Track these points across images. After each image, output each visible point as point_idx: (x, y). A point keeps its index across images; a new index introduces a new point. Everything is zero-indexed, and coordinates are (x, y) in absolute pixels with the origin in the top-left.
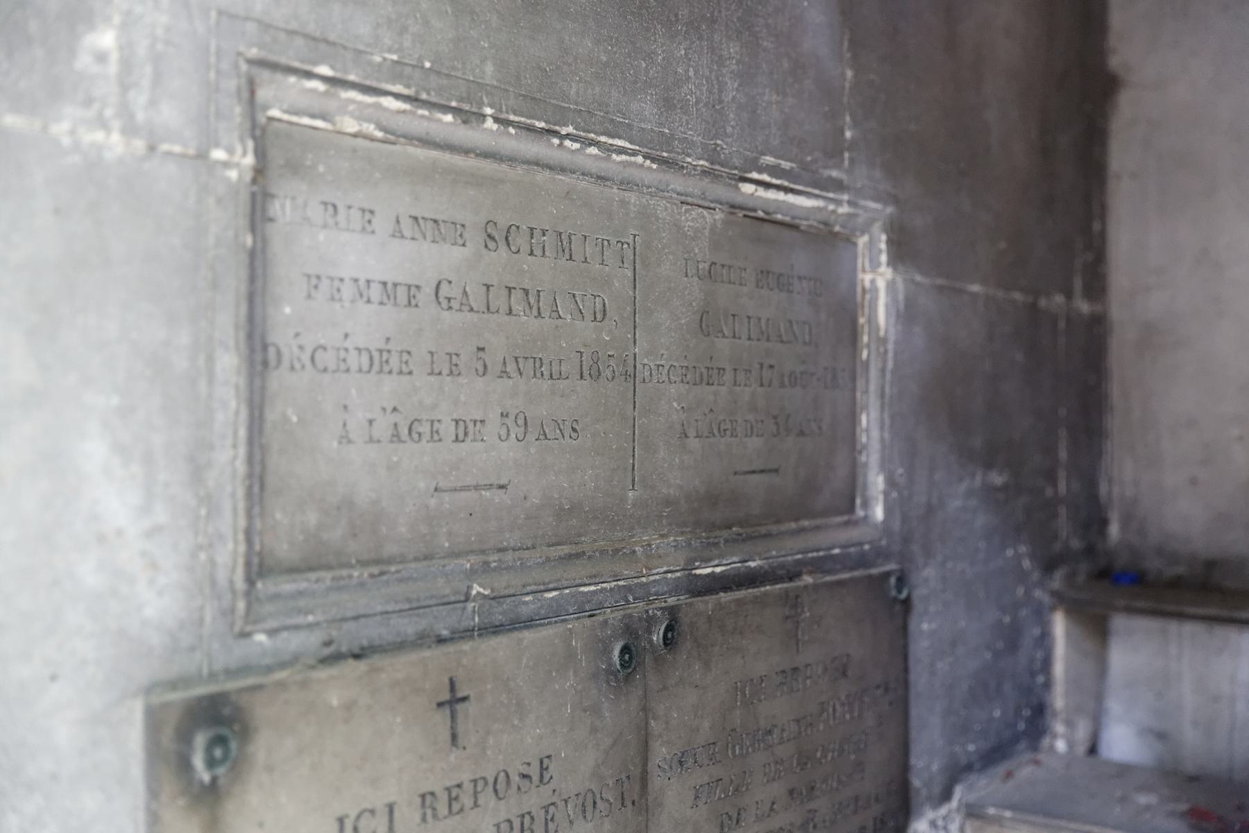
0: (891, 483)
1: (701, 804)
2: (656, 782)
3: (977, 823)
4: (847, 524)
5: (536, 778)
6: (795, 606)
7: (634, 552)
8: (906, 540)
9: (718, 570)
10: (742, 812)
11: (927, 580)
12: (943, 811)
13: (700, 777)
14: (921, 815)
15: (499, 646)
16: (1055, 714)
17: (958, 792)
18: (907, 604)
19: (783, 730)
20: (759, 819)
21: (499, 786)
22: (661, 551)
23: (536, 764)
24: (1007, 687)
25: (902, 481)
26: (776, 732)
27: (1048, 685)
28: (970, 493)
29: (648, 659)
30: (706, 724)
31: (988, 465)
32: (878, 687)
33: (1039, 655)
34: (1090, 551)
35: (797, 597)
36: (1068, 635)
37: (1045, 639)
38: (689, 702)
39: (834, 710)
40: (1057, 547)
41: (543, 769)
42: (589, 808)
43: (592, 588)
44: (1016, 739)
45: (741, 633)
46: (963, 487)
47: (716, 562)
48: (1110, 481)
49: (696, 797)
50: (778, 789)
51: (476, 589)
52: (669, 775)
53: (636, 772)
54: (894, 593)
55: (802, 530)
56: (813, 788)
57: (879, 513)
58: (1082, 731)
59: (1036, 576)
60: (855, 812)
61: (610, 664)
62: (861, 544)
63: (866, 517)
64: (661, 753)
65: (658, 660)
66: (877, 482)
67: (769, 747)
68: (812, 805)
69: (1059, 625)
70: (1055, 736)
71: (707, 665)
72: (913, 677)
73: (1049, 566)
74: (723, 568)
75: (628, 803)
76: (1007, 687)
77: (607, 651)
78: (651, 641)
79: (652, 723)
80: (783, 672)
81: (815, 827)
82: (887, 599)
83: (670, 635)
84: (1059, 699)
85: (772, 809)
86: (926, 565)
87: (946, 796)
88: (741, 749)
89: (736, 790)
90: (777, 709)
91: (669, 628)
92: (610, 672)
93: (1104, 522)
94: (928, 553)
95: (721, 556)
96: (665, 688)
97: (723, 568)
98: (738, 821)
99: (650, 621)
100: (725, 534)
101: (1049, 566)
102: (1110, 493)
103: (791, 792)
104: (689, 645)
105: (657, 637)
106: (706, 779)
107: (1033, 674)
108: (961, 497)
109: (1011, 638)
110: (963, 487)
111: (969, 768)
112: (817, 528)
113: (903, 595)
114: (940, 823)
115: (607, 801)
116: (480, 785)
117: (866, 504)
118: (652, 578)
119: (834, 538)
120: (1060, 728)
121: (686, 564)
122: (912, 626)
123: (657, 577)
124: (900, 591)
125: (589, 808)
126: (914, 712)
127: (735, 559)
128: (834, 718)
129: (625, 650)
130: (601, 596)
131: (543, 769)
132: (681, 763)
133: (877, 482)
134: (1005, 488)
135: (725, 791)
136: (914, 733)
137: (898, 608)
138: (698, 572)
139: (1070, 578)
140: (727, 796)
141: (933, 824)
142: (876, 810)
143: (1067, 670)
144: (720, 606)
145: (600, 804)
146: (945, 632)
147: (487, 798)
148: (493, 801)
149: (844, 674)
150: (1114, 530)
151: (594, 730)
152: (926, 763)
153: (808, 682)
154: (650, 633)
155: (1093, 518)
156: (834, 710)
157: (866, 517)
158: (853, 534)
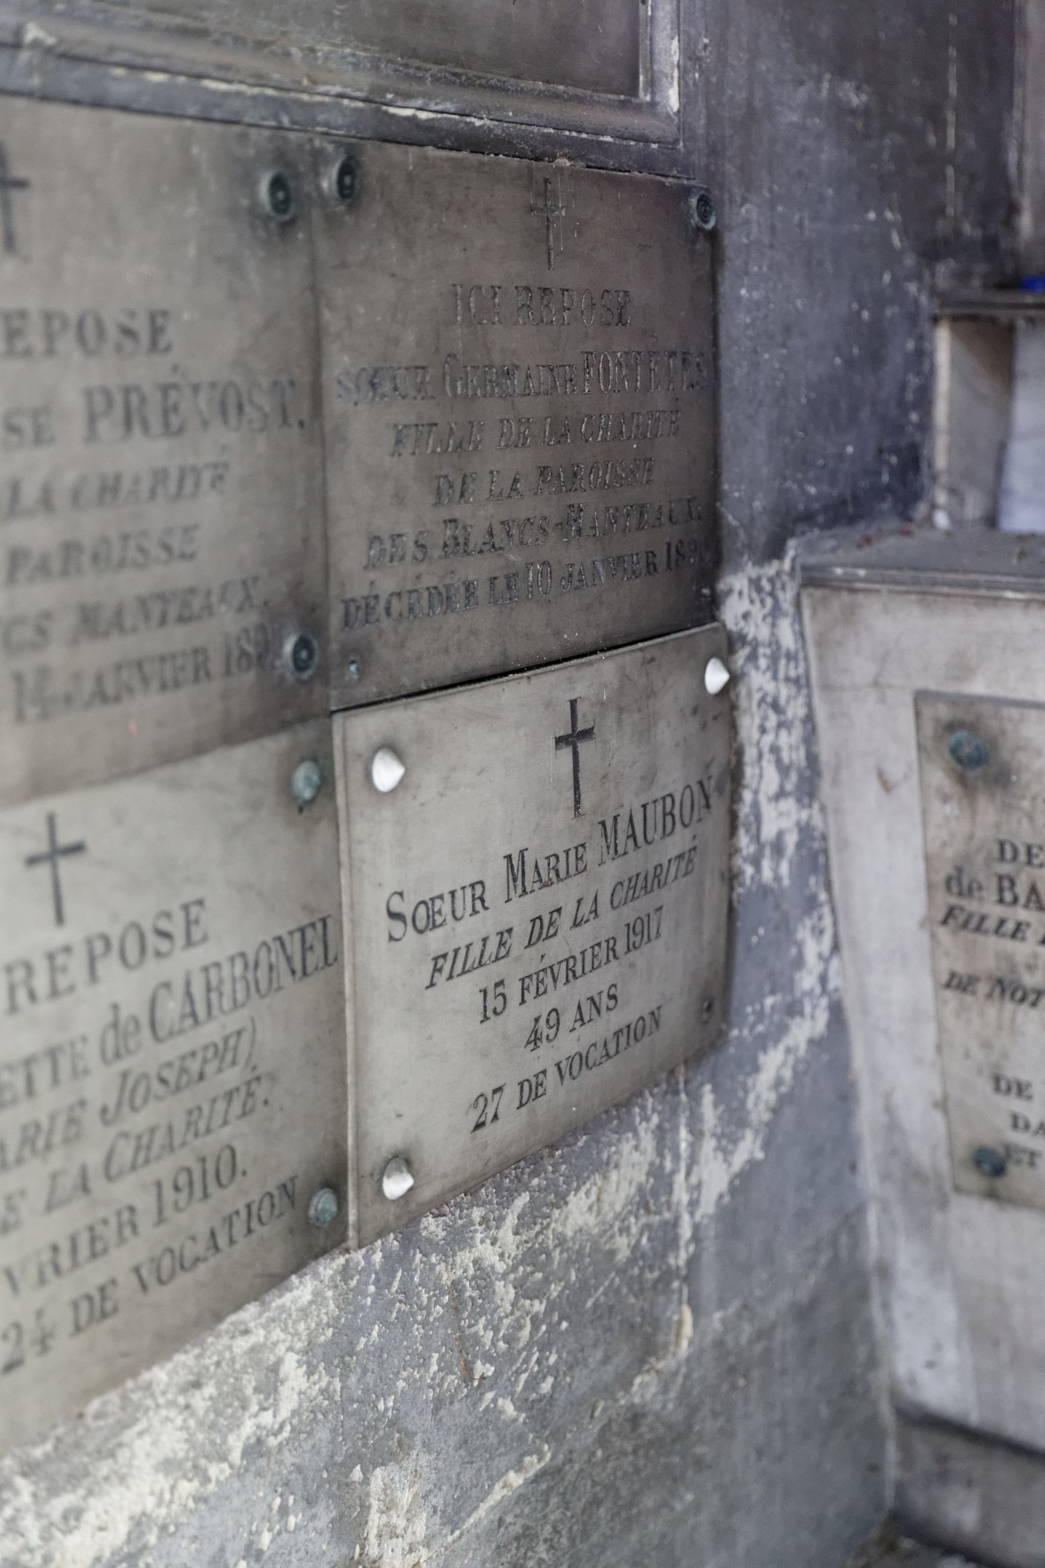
0: (690, 55)
1: (406, 451)
2: (336, 405)
3: (818, 593)
4: (623, 105)
5: (145, 336)
6: (543, 194)
7: (288, 55)
8: (715, 151)
9: (423, 115)
10: (469, 480)
11: (746, 221)
12: (771, 569)
13: (403, 413)
14: (738, 569)
15: (79, 123)
16: (934, 478)
17: (792, 548)
18: (714, 237)
19: (528, 377)
20: (495, 497)
21: (88, 332)
22: (331, 65)
23: (179, 917)
24: (865, 414)
25: (708, 57)
26: (518, 379)
27: (926, 426)
28: (811, 107)
29: (316, 215)
30: (410, 337)
31: (841, 72)
32: (672, 354)
33: (913, 381)
34: (990, 246)
35: (546, 181)
36: (954, 362)
37: (921, 358)
38: (385, 295)
39: (606, 369)
40: (942, 227)
41: (156, 331)
42: (232, 411)
43: (223, 87)
44: (879, 492)
45: (460, 211)
46: (802, 93)
47: (419, 102)
48: (1022, 148)
49: (398, 442)
50: (520, 461)
51: (33, 32)
52: (355, 397)
53: (305, 379)
54: (695, 220)
55: (556, 96)
56: (575, 475)
57: (673, 99)
58: (974, 507)
59: (910, 261)
60: (640, 528)
61: (255, 203)
62: (645, 140)
63: (653, 104)
64: (340, 363)
65: (331, 219)
66: (669, 50)
67: (504, 396)
68: (573, 499)
69: (943, 344)
70: (933, 507)
71: (408, 245)
72: (725, 362)
73: (931, 252)
74: (431, 115)
75: (293, 421)
76: (865, 414)
77: (248, 181)
78: (318, 188)
79: (326, 314)
80: (528, 289)
81: (579, 531)
82: (682, 212)
83: (347, 180)
84: (941, 453)
85: (513, 489)
86: (745, 200)
87: (775, 550)
88: (465, 386)
89: (459, 446)
90: (516, 341)
91: (346, 170)
92: (253, 211)
93: (1013, 210)
94: (749, 186)
95: (428, 96)
96: (343, 265)
97: (431, 115)
98: (462, 494)
99: (318, 158)
100: (435, 68)
101: (931, 252)
102: (1020, 165)
103: (543, 471)
104: (378, 209)
105: (328, 183)
106: (412, 419)
107: (903, 407)
108: (800, 104)
109: (869, 345)
110: (802, 93)
111: (808, 518)
112: (579, 100)
113: (709, 226)
114: (766, 586)
115: (260, 409)
116: (56, 325)
117: (652, 84)
118: (318, 98)
119: (603, 119)
120: (941, 497)
121: (371, 92)
122: (724, 288)
123: (327, 99)
124: (705, 219)
125: (232, 411)
126: (727, 416)
127: (449, 106)
128: (607, 382)
129: (277, 184)
130: (237, 104)
131: (156, 331)
132: (372, 385)
133: (669, 50)
134: (865, 112)
135: (440, 441)
136: (727, 448)
137: (701, 245)
138: (392, 110)
139: (963, 276)
140: (445, 451)
141: (755, 584)
142: (670, 533)
143: (951, 416)
144: (426, 163)
145: (248, 409)
146: (774, 314)
147: (66, 343)
148: (77, 356)
149: (621, 320)
150: (1026, 222)
151: (234, 296)
152: (747, 495)
153: (566, 314)
154: (317, 174)
155: (998, 203)
156: (606, 369)
157: (653, 104)
158: (637, 122)
